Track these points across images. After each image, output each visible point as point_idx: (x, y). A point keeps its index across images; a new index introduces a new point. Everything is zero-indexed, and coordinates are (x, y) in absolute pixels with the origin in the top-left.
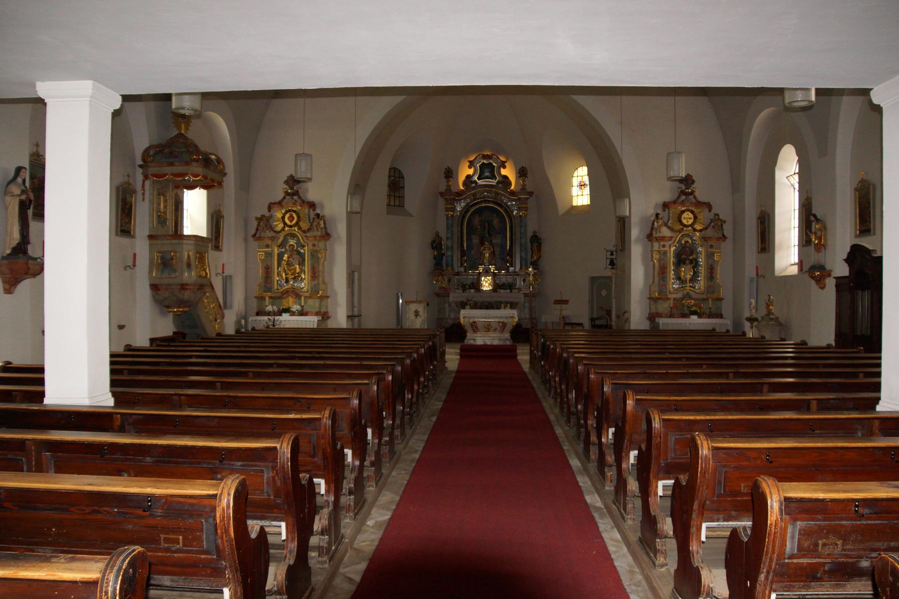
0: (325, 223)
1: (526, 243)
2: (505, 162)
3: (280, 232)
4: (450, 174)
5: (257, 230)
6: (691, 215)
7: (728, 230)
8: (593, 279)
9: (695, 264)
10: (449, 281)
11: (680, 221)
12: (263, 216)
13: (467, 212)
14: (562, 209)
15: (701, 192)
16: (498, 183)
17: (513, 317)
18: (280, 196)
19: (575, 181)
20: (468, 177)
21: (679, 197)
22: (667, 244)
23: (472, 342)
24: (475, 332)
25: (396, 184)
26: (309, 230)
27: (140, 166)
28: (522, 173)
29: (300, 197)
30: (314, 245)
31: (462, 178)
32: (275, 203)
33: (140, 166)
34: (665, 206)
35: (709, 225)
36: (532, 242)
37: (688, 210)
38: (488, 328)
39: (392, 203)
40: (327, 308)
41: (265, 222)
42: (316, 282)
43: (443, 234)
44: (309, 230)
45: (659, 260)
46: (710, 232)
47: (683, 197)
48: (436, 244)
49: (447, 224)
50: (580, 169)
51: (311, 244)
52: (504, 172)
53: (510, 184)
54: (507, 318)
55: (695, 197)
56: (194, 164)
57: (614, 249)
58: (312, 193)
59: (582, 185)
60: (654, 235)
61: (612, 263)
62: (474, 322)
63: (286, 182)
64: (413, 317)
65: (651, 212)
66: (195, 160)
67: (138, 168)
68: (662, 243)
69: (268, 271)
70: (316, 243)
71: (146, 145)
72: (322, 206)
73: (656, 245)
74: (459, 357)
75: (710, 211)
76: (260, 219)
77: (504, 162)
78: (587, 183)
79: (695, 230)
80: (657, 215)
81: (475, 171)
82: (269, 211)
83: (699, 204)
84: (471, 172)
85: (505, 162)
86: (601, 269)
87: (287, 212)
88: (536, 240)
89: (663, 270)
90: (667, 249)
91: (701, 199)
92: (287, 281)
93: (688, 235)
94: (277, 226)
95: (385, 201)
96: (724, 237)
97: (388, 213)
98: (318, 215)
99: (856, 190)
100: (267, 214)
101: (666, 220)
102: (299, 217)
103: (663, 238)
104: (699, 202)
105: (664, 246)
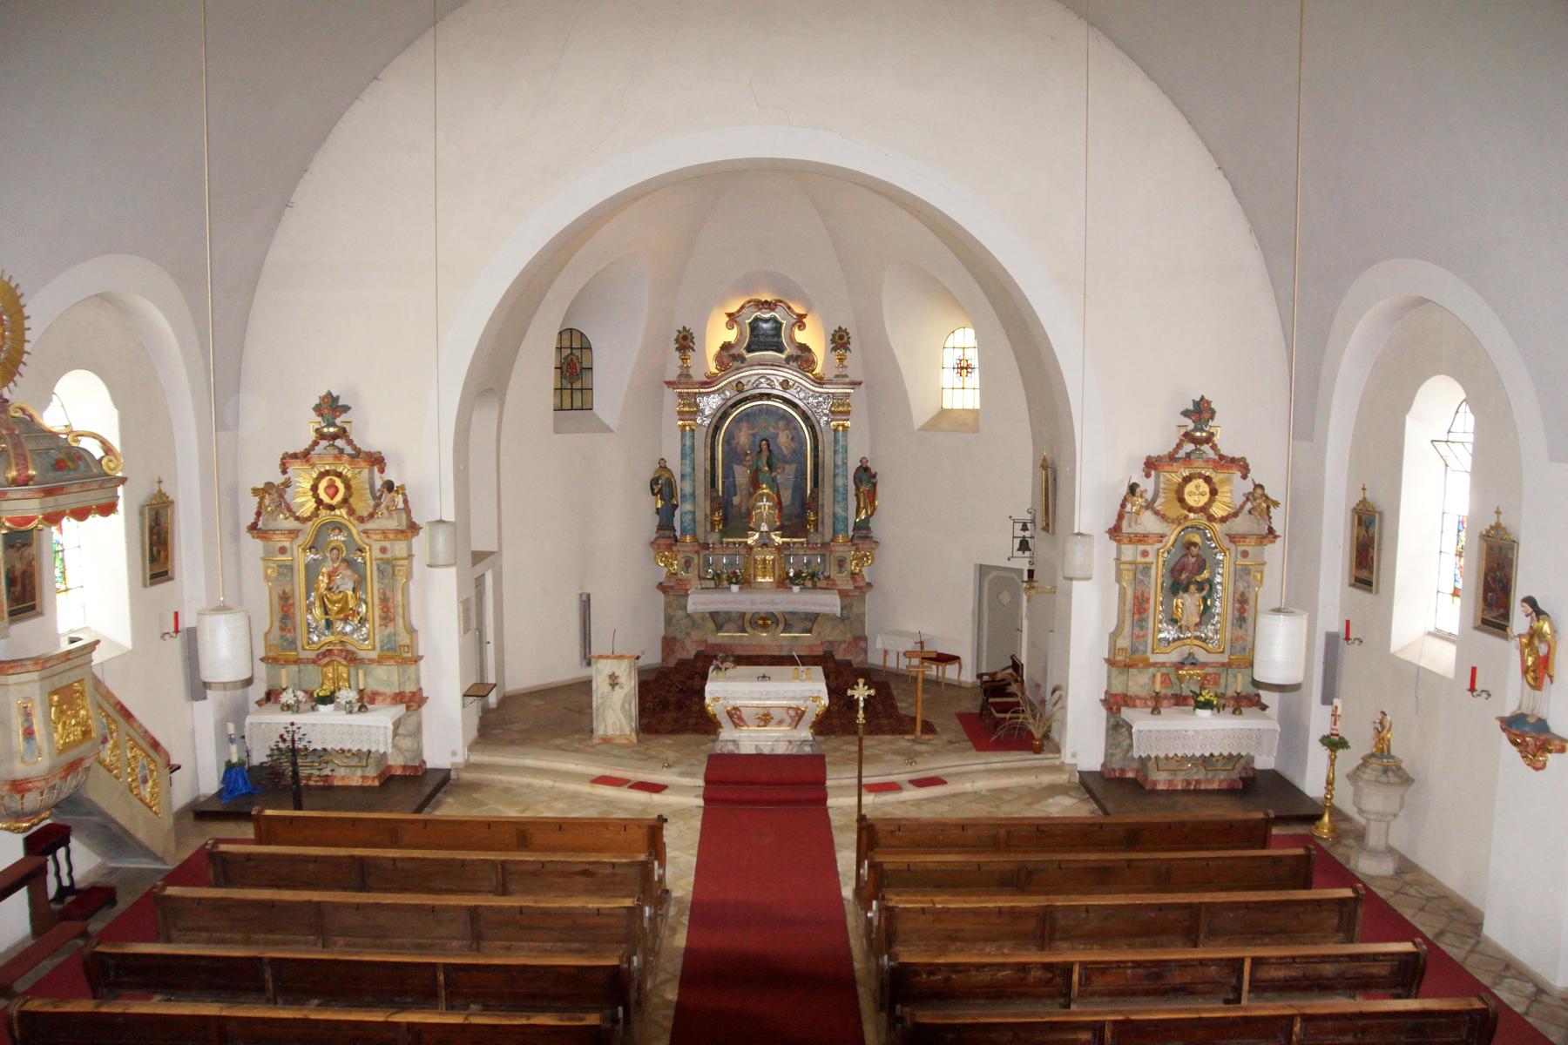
0: (406, 501)
1: (845, 486)
2: (804, 316)
3: (309, 519)
4: (685, 342)
5: (259, 514)
6: (1205, 488)
7: (1278, 519)
8: (983, 570)
9: (1207, 588)
10: (688, 563)
11: (1181, 500)
12: (269, 485)
13: (725, 415)
14: (921, 413)
15: (1228, 436)
16: (789, 359)
17: (816, 699)
20: (726, 347)
21: (1179, 446)
22: (1151, 549)
23: (730, 748)
24: (736, 726)
25: (573, 369)
28: (840, 341)
29: (350, 442)
30: (383, 550)
31: (713, 348)
32: (295, 456)
34: (1151, 465)
35: (1242, 507)
36: (858, 481)
37: (1200, 476)
38: (765, 719)
39: (567, 404)
40: (418, 680)
41: (273, 495)
42: (390, 629)
43: (675, 465)
44: (371, 516)
47: (1189, 447)
48: (662, 486)
49: (683, 445)
50: (959, 332)
51: (376, 547)
52: (801, 337)
54: (806, 699)
55: (1214, 447)
56: (15, 492)
57: (1028, 517)
58: (370, 433)
59: (963, 368)
61: (1024, 546)
62: (736, 709)
64: (607, 688)
66: (15, 482)
68: (1141, 547)
69: (285, 606)
70: (387, 544)
73: (1129, 552)
74: (701, 802)
75: (1244, 477)
77: (801, 317)
78: (975, 362)
79: (1211, 518)
80: (1133, 488)
81: (741, 334)
82: (284, 472)
84: (731, 336)
85: (804, 316)
86: (1001, 551)
87: (322, 475)
88: (865, 476)
89: (1140, 605)
90: (1150, 559)
91: (1228, 450)
92: (329, 624)
93: (1196, 528)
94: (302, 505)
95: (549, 399)
97: (557, 431)
98: (389, 486)
100: (278, 479)
101: (1149, 496)
102: (348, 487)
104: (1222, 457)
105: (1145, 554)
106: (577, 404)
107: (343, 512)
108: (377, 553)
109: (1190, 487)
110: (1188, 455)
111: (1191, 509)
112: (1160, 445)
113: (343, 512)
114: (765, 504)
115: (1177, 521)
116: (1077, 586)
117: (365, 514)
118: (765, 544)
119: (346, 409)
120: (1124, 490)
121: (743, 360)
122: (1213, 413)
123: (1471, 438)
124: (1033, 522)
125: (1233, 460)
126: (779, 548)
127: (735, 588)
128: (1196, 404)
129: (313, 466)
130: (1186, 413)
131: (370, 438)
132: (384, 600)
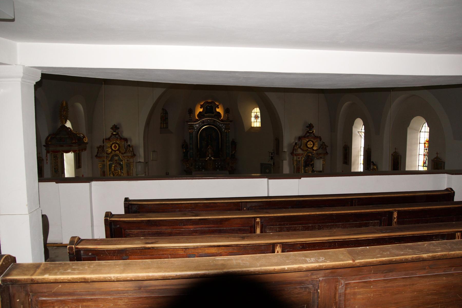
0: (133, 149)
3: (110, 154)
4: (191, 111)
5: (98, 153)
6: (312, 143)
7: (328, 150)
12: (100, 146)
14: (246, 129)
16: (215, 115)
18: (109, 135)
19: (253, 115)
20: (200, 112)
21: (306, 134)
22: (300, 157)
25: (165, 118)
26: (125, 153)
27: (44, 146)
28: (227, 111)
29: (119, 136)
30: (128, 160)
33: (44, 146)
34: (300, 138)
37: (311, 141)
41: (101, 148)
45: (297, 165)
46: (320, 151)
47: (308, 134)
50: (255, 109)
52: (218, 110)
53: (220, 116)
55: (314, 134)
60: (295, 153)
61: (272, 158)
63: (112, 128)
65: (293, 141)
66: (74, 143)
67: (43, 147)
71: (47, 135)
72: (131, 140)
73: (295, 158)
75: (320, 141)
76: (98, 148)
78: (260, 116)
79: (313, 150)
80: (296, 143)
83: (316, 137)
88: (234, 143)
91: (316, 135)
93: (310, 152)
96: (327, 153)
98: (129, 146)
99: (392, 155)
100: (102, 144)
101: (300, 145)
102: (119, 146)
103: (299, 155)
104: (315, 136)
105: (299, 158)
106: (165, 127)
107: (118, 152)
108: (126, 161)
109: (309, 143)
110: (308, 136)
111: (309, 148)
112: (300, 134)
113: (118, 152)
114: (210, 151)
115: (306, 151)
116: (284, 161)
117: (123, 152)
118: (210, 159)
119: (118, 128)
120: (294, 144)
121: (204, 116)
122: (313, 127)
123: (364, 131)
124: (274, 153)
125: (318, 137)
126: (214, 160)
127: (203, 170)
128: (309, 125)
129: (111, 141)
130: (307, 127)
131: (125, 134)
132: (128, 172)
